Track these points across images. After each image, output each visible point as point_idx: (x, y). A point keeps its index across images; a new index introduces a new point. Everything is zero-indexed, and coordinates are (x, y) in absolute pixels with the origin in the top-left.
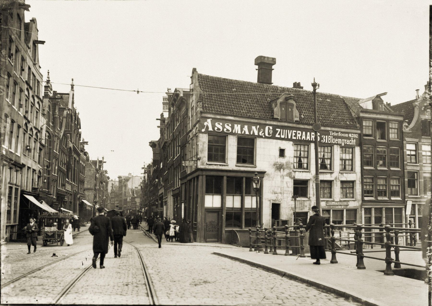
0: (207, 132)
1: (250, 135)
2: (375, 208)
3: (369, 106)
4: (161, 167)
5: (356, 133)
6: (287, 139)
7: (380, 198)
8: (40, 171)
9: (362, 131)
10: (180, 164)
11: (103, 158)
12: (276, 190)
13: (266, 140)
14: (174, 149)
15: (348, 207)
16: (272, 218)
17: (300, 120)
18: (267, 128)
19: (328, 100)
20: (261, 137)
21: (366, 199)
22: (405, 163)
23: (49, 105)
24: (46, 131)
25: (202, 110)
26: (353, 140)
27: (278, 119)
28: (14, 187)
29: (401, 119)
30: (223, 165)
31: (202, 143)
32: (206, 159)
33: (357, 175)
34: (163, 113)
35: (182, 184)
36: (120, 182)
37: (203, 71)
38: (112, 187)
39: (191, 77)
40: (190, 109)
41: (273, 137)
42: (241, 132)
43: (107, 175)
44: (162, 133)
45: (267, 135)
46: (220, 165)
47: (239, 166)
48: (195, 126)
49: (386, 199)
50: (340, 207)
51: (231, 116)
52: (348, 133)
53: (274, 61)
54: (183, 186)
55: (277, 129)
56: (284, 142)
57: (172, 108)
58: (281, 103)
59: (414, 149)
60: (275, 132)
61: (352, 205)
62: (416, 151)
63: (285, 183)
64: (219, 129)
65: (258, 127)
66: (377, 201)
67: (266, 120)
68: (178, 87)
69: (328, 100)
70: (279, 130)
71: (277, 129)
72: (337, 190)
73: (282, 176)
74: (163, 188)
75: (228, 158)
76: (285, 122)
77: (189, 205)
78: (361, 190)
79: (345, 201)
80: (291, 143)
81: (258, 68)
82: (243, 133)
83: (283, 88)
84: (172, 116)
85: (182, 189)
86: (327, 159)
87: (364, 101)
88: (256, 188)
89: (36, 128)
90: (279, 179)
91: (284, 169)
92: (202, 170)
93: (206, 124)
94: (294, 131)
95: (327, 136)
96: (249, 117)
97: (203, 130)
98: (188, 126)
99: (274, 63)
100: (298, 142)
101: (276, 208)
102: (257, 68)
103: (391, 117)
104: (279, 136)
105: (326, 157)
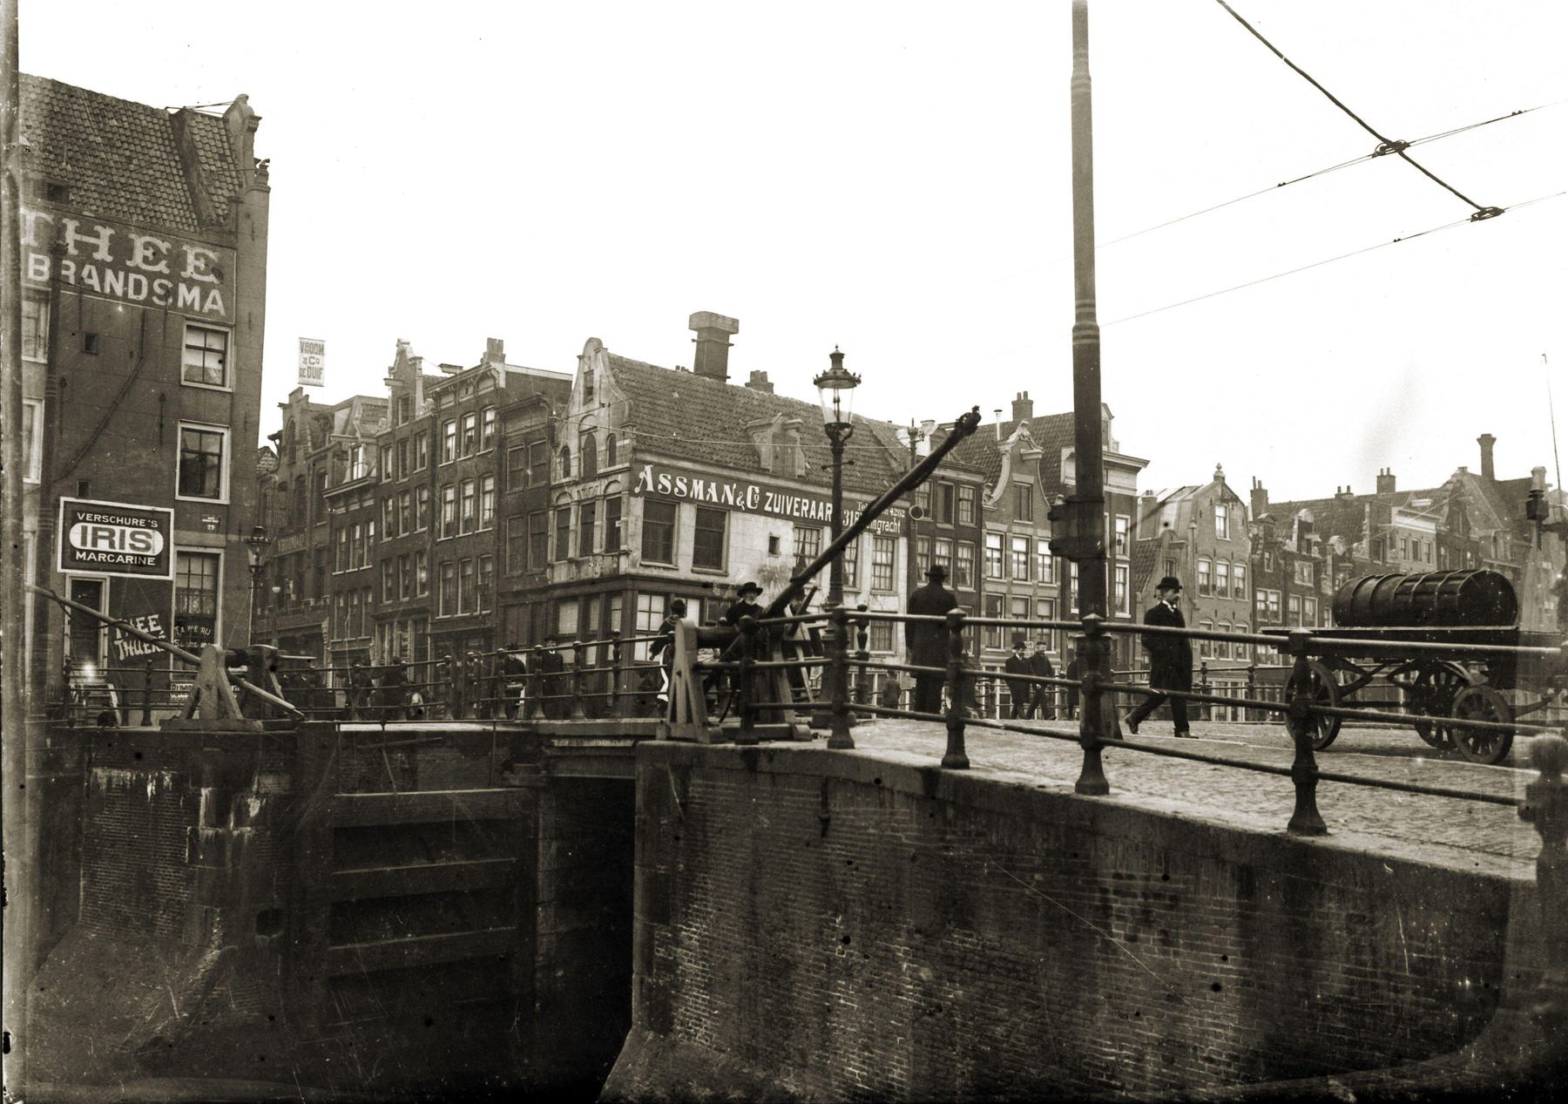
0: (644, 492)
13: (748, 516)
18: (750, 488)
22: (983, 576)
27: (768, 470)
29: (978, 479)
31: (634, 519)
32: (637, 554)
34: (300, 389)
39: (580, 357)
41: (760, 511)
42: (705, 496)
45: (749, 505)
46: (665, 568)
47: (698, 573)
53: (734, 326)
55: (768, 494)
56: (779, 522)
59: (1024, 549)
60: (764, 499)
62: (1000, 550)
64: (665, 488)
67: (748, 472)
71: (768, 494)
75: (680, 552)
80: (791, 524)
81: (699, 337)
86: (849, 562)
91: (775, 582)
93: (642, 475)
97: (637, 490)
103: (964, 477)
104: (769, 509)
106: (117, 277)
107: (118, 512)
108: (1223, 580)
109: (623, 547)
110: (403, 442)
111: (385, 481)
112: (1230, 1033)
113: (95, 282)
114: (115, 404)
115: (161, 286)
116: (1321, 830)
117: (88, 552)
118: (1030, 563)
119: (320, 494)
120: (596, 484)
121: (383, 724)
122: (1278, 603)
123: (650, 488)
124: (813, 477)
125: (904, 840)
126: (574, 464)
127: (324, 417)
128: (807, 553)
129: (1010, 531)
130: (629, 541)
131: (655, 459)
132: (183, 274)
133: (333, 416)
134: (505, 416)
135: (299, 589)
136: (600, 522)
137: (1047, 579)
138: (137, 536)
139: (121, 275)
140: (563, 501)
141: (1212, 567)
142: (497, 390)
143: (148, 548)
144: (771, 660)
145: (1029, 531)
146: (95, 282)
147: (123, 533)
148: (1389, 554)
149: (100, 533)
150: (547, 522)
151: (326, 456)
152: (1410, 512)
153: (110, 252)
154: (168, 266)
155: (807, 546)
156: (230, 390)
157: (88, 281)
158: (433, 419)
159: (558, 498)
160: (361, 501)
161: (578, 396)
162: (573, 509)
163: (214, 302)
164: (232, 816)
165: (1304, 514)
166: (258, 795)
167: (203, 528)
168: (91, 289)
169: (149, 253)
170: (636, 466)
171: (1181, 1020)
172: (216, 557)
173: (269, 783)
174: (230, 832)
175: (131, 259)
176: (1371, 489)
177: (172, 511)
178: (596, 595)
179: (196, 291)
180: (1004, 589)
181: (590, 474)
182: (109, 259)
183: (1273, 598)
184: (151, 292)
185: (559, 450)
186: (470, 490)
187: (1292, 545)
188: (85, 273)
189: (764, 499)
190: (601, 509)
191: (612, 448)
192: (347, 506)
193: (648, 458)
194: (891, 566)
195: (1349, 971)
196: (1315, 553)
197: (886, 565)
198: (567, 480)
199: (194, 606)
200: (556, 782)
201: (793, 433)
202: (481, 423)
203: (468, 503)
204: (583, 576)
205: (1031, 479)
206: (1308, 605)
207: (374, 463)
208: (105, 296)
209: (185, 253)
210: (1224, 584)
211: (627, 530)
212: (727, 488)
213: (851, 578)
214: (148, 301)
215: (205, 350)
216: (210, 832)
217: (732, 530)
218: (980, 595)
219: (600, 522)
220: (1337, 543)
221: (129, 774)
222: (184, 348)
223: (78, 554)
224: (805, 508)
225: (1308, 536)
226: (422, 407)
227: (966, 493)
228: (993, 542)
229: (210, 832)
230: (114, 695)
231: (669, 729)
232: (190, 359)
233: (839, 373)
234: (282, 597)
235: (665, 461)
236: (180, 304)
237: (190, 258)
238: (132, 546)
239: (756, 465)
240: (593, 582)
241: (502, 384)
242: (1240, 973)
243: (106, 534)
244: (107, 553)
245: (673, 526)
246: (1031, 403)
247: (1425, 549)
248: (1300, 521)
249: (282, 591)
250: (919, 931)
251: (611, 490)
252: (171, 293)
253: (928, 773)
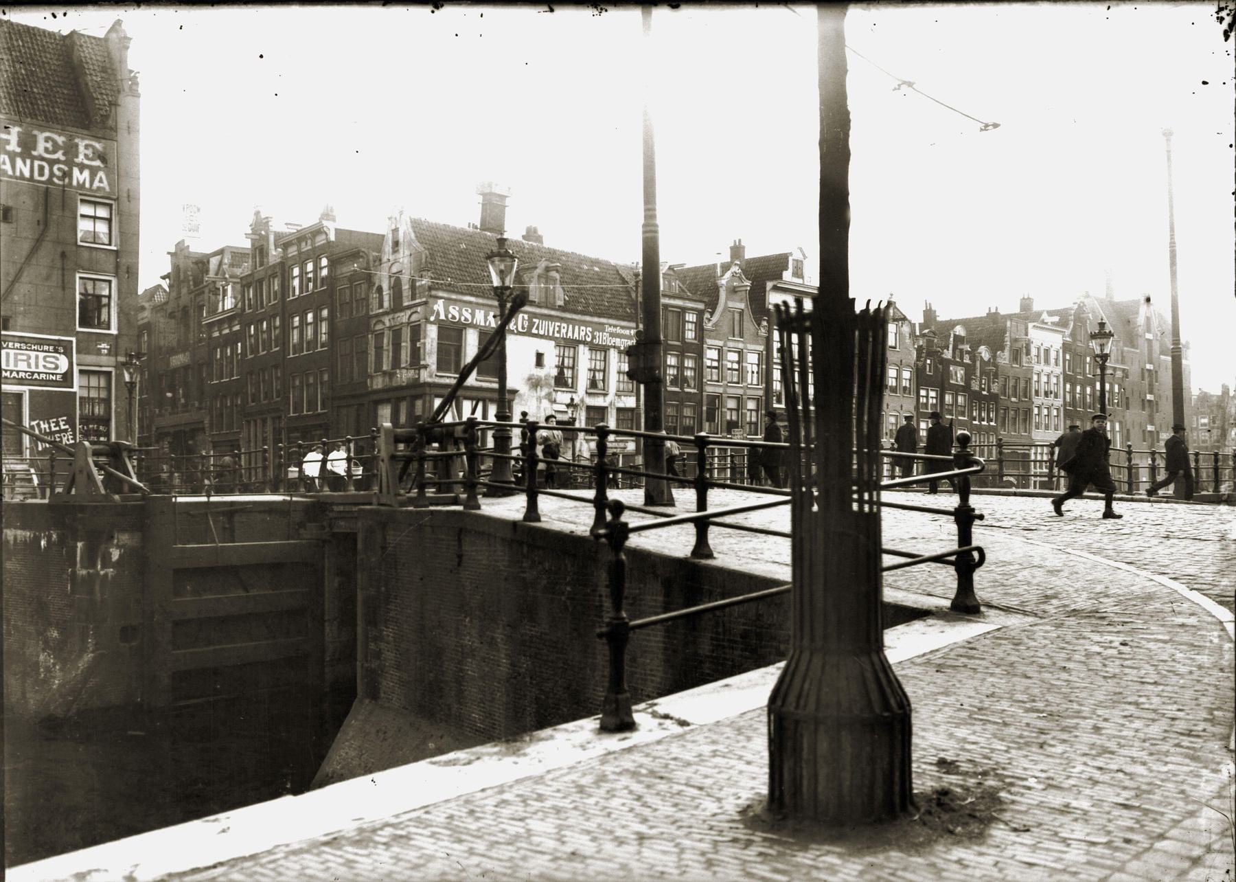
13: (519, 338)
22: (705, 380)
41: (528, 333)
42: (485, 322)
45: (520, 329)
60: (531, 325)
64: (454, 317)
93: (436, 307)
97: (432, 319)
103: (689, 304)
104: (536, 332)
107: (32, 341)
108: (894, 380)
109: (422, 363)
110: (260, 282)
111: (248, 311)
112: (659, 680)
115: (59, 169)
116: (710, 556)
118: (741, 371)
119: (200, 322)
120: (402, 314)
121: (208, 496)
122: (936, 398)
124: (571, 307)
125: (502, 568)
126: (386, 298)
127: (202, 263)
128: (566, 364)
129: (725, 345)
130: (427, 357)
131: (445, 295)
132: (76, 160)
133: (208, 262)
134: (333, 264)
135: (186, 396)
136: (406, 345)
137: (755, 382)
138: (48, 359)
139: (28, 162)
140: (379, 327)
141: (899, 373)
142: (329, 242)
143: (57, 368)
144: (446, 450)
145: (741, 346)
147: (37, 357)
148: (1024, 359)
150: (367, 343)
151: (203, 292)
152: (1043, 326)
153: (19, 145)
154: (64, 154)
155: (566, 360)
156: (115, 248)
158: (282, 264)
159: (375, 324)
160: (230, 327)
161: (388, 247)
162: (386, 332)
163: (101, 181)
164: (99, 562)
165: (959, 330)
166: (118, 547)
169: (49, 145)
170: (431, 300)
171: (636, 673)
173: (124, 538)
174: (98, 573)
175: (35, 150)
176: (1016, 309)
178: (404, 398)
179: (86, 173)
180: (721, 390)
181: (397, 307)
183: (933, 394)
184: (52, 174)
185: (375, 288)
186: (310, 317)
187: (948, 354)
189: (531, 325)
190: (406, 334)
191: (413, 287)
192: (220, 331)
193: (441, 294)
195: (712, 639)
196: (967, 360)
198: (381, 311)
200: (334, 535)
201: (554, 274)
202: (317, 268)
203: (309, 327)
204: (394, 384)
205: (742, 306)
206: (960, 399)
207: (239, 297)
209: (77, 145)
210: (894, 384)
211: (425, 349)
214: (50, 181)
215: (95, 218)
216: (84, 572)
218: (702, 396)
219: (406, 345)
220: (984, 352)
221: (28, 534)
222: (79, 218)
224: (564, 331)
225: (961, 347)
226: (274, 254)
227: (691, 317)
228: (711, 354)
229: (84, 572)
230: (35, 477)
231: (378, 498)
232: (84, 226)
233: (502, 251)
234: (174, 400)
235: (454, 296)
236: (75, 183)
237: (81, 149)
238: (44, 366)
240: (401, 388)
241: (332, 238)
242: (664, 643)
243: (25, 358)
244: (26, 372)
246: (744, 247)
247: (1053, 355)
248: (955, 335)
249: (174, 396)
250: (508, 625)
251: (414, 317)
252: (67, 175)
253: (514, 524)
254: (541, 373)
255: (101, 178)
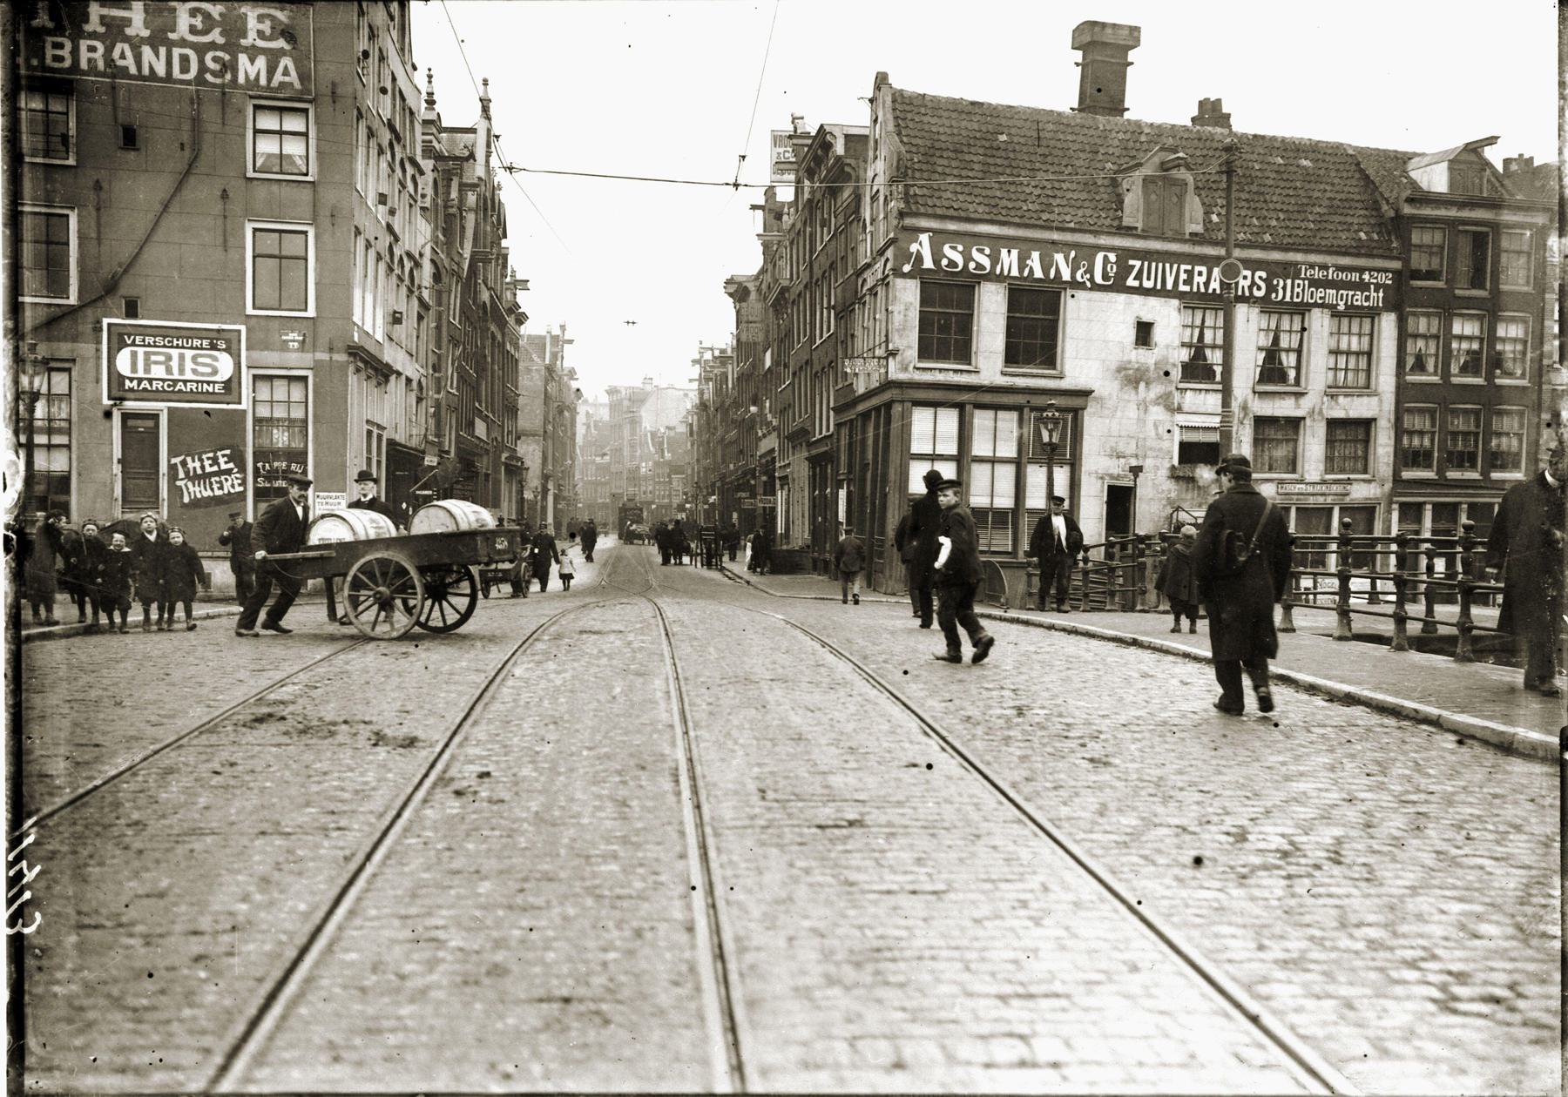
0: (918, 272)
1: (1046, 279)
2: (1436, 506)
3: (1436, 180)
4: (768, 363)
5: (1386, 271)
6: (1161, 293)
7: (1452, 474)
8: (420, 383)
9: (1406, 261)
10: (832, 365)
11: (563, 328)
12: (1121, 448)
14: (813, 315)
15: (1347, 499)
16: (1108, 529)
17: (1206, 230)
18: (1100, 257)
19: (1305, 163)
20: (1080, 286)
21: (1407, 474)
23: (435, 181)
24: (432, 261)
25: (902, 205)
26: (1376, 291)
28: (375, 431)
30: (962, 371)
31: (902, 308)
32: (913, 353)
33: (1381, 401)
34: (771, 188)
35: (838, 426)
36: (614, 407)
37: (906, 81)
38: (588, 426)
39: (871, 101)
40: (868, 199)
42: (1021, 270)
43: (574, 385)
44: (770, 253)
45: (1098, 279)
46: (955, 371)
48: (882, 252)
49: (1475, 475)
50: (1321, 499)
51: (992, 222)
52: (1361, 270)
53: (1133, 36)
54: (845, 431)
55: (1131, 262)
56: (1153, 301)
57: (807, 183)
58: (1147, 181)
60: (1124, 271)
61: (1361, 492)
63: (1150, 425)
64: (952, 263)
65: (1073, 254)
66: (1442, 484)
67: (1095, 233)
68: (829, 119)
69: (1305, 163)
70: (1138, 264)
71: (1131, 262)
72: (1313, 446)
73: (1144, 406)
74: (775, 434)
76: (1157, 238)
77: (863, 489)
78: (1391, 450)
79: (1336, 482)
80: (1175, 302)
81: (1084, 58)
82: (1026, 274)
83: (1159, 126)
84: (810, 209)
85: (839, 440)
86: (1288, 351)
87: (1426, 160)
88: (1050, 444)
89: (409, 255)
90: (1132, 412)
92: (900, 385)
93: (914, 248)
94: (1183, 267)
95: (1289, 282)
96: (1047, 227)
97: (907, 268)
98: (861, 249)
99: (1136, 43)
100: (1195, 301)
101: (1120, 501)
102: (1080, 60)
104: (1136, 284)
105: (1284, 344)
106: (157, 55)
113: (129, 62)
114: (166, 207)
115: (215, 59)
117: (140, 380)
123: (928, 263)
138: (200, 360)
146: (129, 62)
147: (182, 357)
149: (153, 358)
154: (222, 34)
157: (121, 63)
163: (286, 73)
167: (284, 346)
168: (124, 72)
172: (305, 379)
175: (173, 31)
177: (243, 328)
182: (146, 33)
184: (203, 69)
188: (116, 54)
193: (924, 223)
194: (1369, 354)
197: (1358, 354)
199: (281, 438)
208: (144, 78)
212: (1059, 258)
213: (1292, 374)
214: (200, 80)
217: (1069, 316)
218: (1540, 390)
223: (127, 382)
236: (241, 79)
237: (252, 24)
238: (194, 371)
239: (1115, 223)
243: (162, 358)
244: (163, 380)
245: (1057, 321)
252: (232, 67)
254: (1146, 357)
255: (286, 67)
